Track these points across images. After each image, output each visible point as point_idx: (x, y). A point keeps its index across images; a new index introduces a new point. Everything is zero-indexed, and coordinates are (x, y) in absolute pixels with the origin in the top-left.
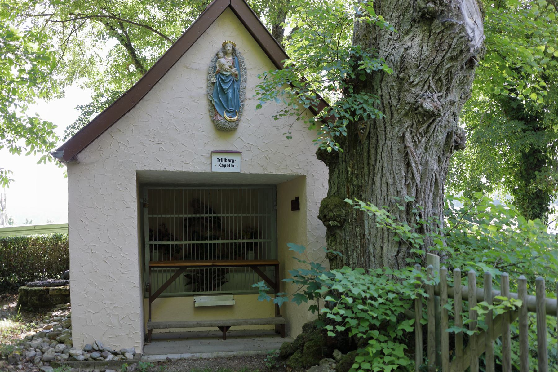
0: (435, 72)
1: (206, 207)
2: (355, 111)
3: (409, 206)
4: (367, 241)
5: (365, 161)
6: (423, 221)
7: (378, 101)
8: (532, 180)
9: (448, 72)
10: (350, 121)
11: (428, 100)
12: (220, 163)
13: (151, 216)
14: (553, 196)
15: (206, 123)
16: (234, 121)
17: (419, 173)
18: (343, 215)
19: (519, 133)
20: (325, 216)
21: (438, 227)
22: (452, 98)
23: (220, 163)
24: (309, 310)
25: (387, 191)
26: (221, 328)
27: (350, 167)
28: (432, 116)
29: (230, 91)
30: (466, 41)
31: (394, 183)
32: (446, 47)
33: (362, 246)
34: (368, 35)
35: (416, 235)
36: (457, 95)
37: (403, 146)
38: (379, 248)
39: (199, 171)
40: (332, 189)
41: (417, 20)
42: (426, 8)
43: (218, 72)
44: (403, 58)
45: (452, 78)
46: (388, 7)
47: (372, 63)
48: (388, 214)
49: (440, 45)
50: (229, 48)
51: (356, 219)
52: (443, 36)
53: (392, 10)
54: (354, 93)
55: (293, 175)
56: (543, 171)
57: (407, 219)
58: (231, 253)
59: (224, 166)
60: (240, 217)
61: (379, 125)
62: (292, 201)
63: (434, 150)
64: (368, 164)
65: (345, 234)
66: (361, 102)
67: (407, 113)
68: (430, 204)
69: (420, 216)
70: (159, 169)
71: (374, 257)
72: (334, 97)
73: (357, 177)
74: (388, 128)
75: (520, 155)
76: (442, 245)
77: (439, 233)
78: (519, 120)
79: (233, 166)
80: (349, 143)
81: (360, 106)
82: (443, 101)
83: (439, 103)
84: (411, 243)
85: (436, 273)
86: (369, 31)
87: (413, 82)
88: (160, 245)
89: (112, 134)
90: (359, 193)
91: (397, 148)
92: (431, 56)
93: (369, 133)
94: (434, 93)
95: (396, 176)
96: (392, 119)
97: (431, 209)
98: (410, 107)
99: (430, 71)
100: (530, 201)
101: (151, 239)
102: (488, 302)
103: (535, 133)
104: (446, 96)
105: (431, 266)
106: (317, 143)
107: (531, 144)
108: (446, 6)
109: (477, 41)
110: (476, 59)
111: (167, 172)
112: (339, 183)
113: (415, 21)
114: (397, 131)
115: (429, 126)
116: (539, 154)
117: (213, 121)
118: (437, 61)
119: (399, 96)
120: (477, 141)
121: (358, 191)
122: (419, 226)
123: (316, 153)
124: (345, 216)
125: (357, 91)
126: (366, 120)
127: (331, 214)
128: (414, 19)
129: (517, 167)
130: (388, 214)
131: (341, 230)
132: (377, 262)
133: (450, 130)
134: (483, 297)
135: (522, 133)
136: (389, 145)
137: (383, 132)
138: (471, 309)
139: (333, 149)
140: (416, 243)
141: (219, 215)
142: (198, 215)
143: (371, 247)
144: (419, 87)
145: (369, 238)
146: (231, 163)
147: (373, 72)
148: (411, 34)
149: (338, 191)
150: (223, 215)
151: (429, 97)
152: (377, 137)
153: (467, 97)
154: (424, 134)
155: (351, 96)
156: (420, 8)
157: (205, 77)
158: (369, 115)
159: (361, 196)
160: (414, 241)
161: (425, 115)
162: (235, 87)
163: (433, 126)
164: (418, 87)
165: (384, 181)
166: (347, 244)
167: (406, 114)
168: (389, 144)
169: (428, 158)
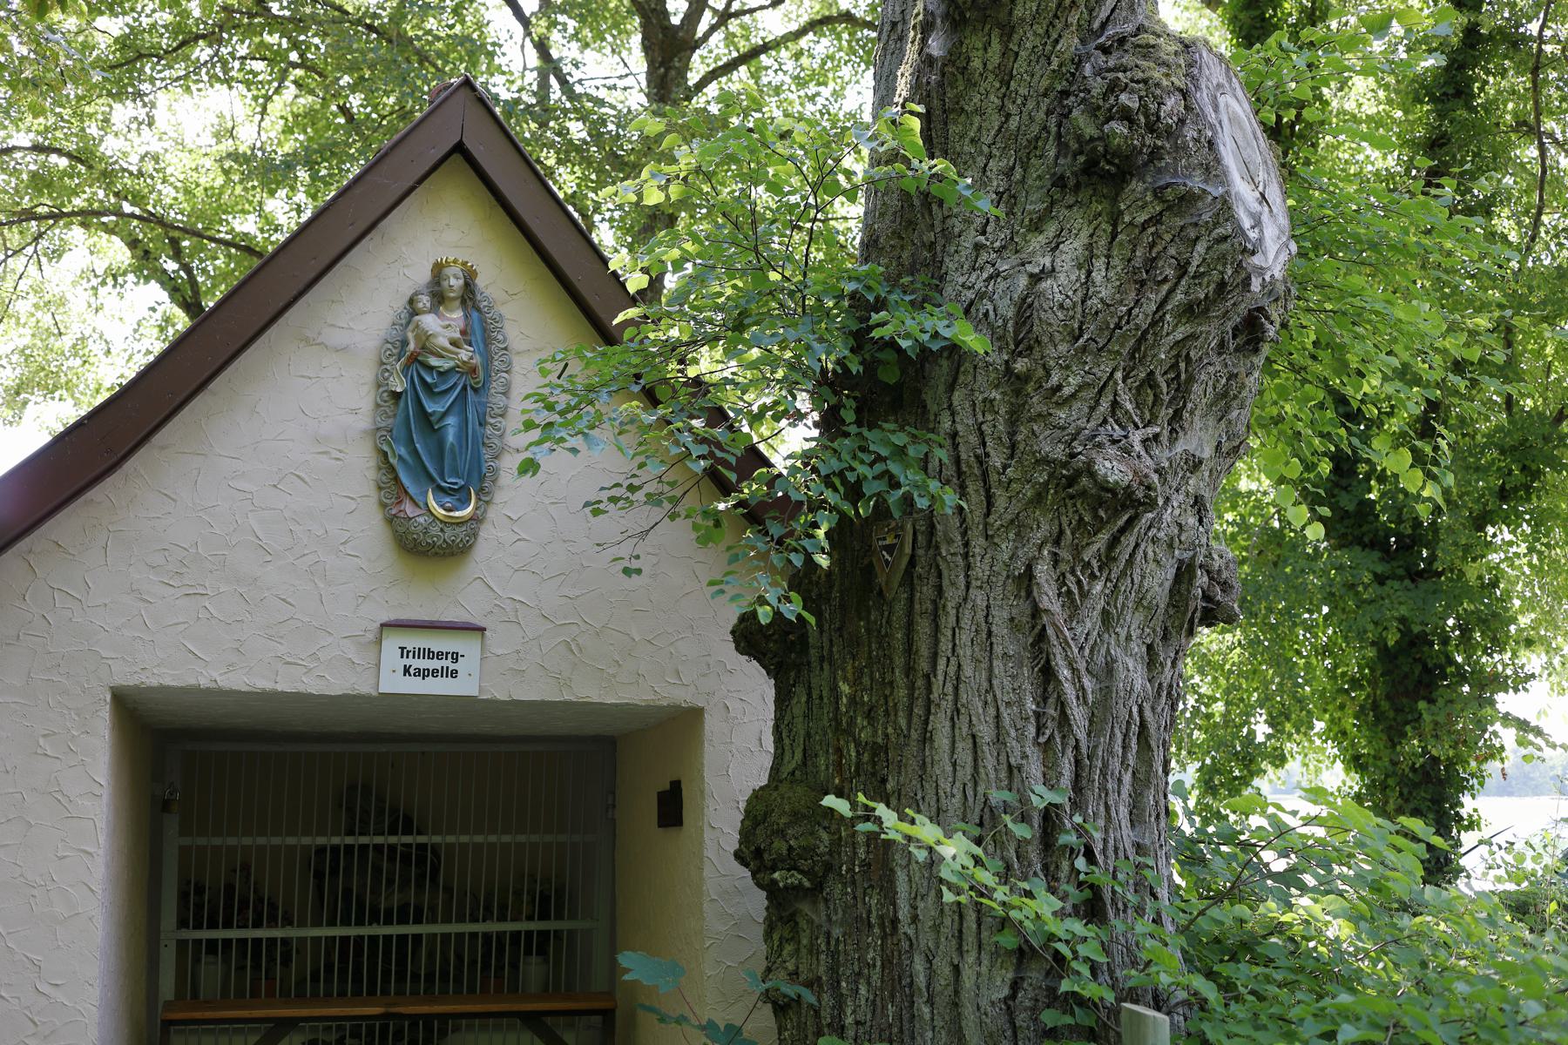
0: (1132, 357)
1: (394, 811)
2: (859, 482)
3: (1050, 818)
4: (905, 945)
5: (899, 661)
6: (1100, 876)
7: (942, 454)
8: (1408, 728)
9: (1178, 356)
11: (1112, 451)
12: (408, 662)
13: (186, 841)
14: (1473, 775)
16: (461, 523)
17: (1085, 702)
19: (1366, 587)
20: (758, 853)
21: (1154, 896)
22: (1191, 448)
23: (408, 662)
27: (845, 679)
28: (1124, 507)
29: (451, 421)
30: (1236, 249)
31: (999, 739)
32: (1170, 272)
33: (887, 963)
34: (910, 228)
35: (1077, 927)
36: (1206, 437)
37: (1026, 607)
38: (947, 971)
40: (787, 757)
41: (1072, 182)
42: (1099, 139)
43: (414, 359)
44: (1025, 309)
45: (1191, 379)
48: (979, 851)
49: (1151, 263)
50: (453, 281)
51: (866, 865)
52: (1156, 235)
53: (986, 149)
55: (661, 708)
56: (1441, 702)
57: (1045, 868)
59: (423, 674)
60: (492, 846)
61: (945, 534)
63: (1133, 621)
64: (909, 670)
65: (830, 920)
66: (884, 452)
68: (1124, 811)
70: (192, 681)
71: (930, 1001)
72: (789, 443)
73: (870, 715)
74: (978, 544)
75: (1371, 653)
76: (1169, 971)
77: (1157, 921)
78: (1364, 547)
79: (454, 674)
81: (879, 468)
82: (1163, 454)
83: (1149, 462)
84: (1058, 957)
86: (910, 222)
87: (1059, 387)
88: (227, 943)
89: (31, 558)
90: (876, 776)
91: (1006, 615)
92: (1121, 302)
93: (912, 562)
94: (1131, 428)
95: (1005, 713)
96: (988, 514)
98: (1051, 475)
100: (1405, 791)
101: (183, 923)
103: (1411, 586)
106: (722, 591)
107: (1403, 620)
108: (1169, 133)
109: (1271, 256)
110: (1267, 318)
111: (221, 692)
112: (808, 735)
114: (1006, 557)
115: (1114, 541)
116: (1426, 649)
117: (390, 520)
118: (1142, 318)
119: (1012, 434)
121: (874, 764)
122: (1088, 893)
123: (733, 632)
124: (830, 853)
125: (868, 415)
126: (896, 514)
127: (780, 846)
128: (1062, 177)
129: (1362, 687)
130: (979, 851)
131: (815, 903)
132: (939, 1023)
133: (1187, 555)
135: (1375, 585)
136: (977, 607)
139: (777, 614)
141: (437, 839)
142: (364, 840)
143: (919, 966)
145: (911, 932)
147: (924, 351)
148: (1051, 229)
149: (804, 764)
150: (451, 839)
151: (1114, 442)
152: (940, 576)
153: (1236, 449)
154: (1100, 569)
155: (846, 435)
156: (1079, 138)
157: (368, 374)
158: (908, 500)
159: (884, 781)
160: (1075, 952)
162: (470, 409)
163: (1129, 540)
164: (1076, 405)
165: (965, 730)
166: (834, 955)
167: (1039, 499)
168: (981, 602)
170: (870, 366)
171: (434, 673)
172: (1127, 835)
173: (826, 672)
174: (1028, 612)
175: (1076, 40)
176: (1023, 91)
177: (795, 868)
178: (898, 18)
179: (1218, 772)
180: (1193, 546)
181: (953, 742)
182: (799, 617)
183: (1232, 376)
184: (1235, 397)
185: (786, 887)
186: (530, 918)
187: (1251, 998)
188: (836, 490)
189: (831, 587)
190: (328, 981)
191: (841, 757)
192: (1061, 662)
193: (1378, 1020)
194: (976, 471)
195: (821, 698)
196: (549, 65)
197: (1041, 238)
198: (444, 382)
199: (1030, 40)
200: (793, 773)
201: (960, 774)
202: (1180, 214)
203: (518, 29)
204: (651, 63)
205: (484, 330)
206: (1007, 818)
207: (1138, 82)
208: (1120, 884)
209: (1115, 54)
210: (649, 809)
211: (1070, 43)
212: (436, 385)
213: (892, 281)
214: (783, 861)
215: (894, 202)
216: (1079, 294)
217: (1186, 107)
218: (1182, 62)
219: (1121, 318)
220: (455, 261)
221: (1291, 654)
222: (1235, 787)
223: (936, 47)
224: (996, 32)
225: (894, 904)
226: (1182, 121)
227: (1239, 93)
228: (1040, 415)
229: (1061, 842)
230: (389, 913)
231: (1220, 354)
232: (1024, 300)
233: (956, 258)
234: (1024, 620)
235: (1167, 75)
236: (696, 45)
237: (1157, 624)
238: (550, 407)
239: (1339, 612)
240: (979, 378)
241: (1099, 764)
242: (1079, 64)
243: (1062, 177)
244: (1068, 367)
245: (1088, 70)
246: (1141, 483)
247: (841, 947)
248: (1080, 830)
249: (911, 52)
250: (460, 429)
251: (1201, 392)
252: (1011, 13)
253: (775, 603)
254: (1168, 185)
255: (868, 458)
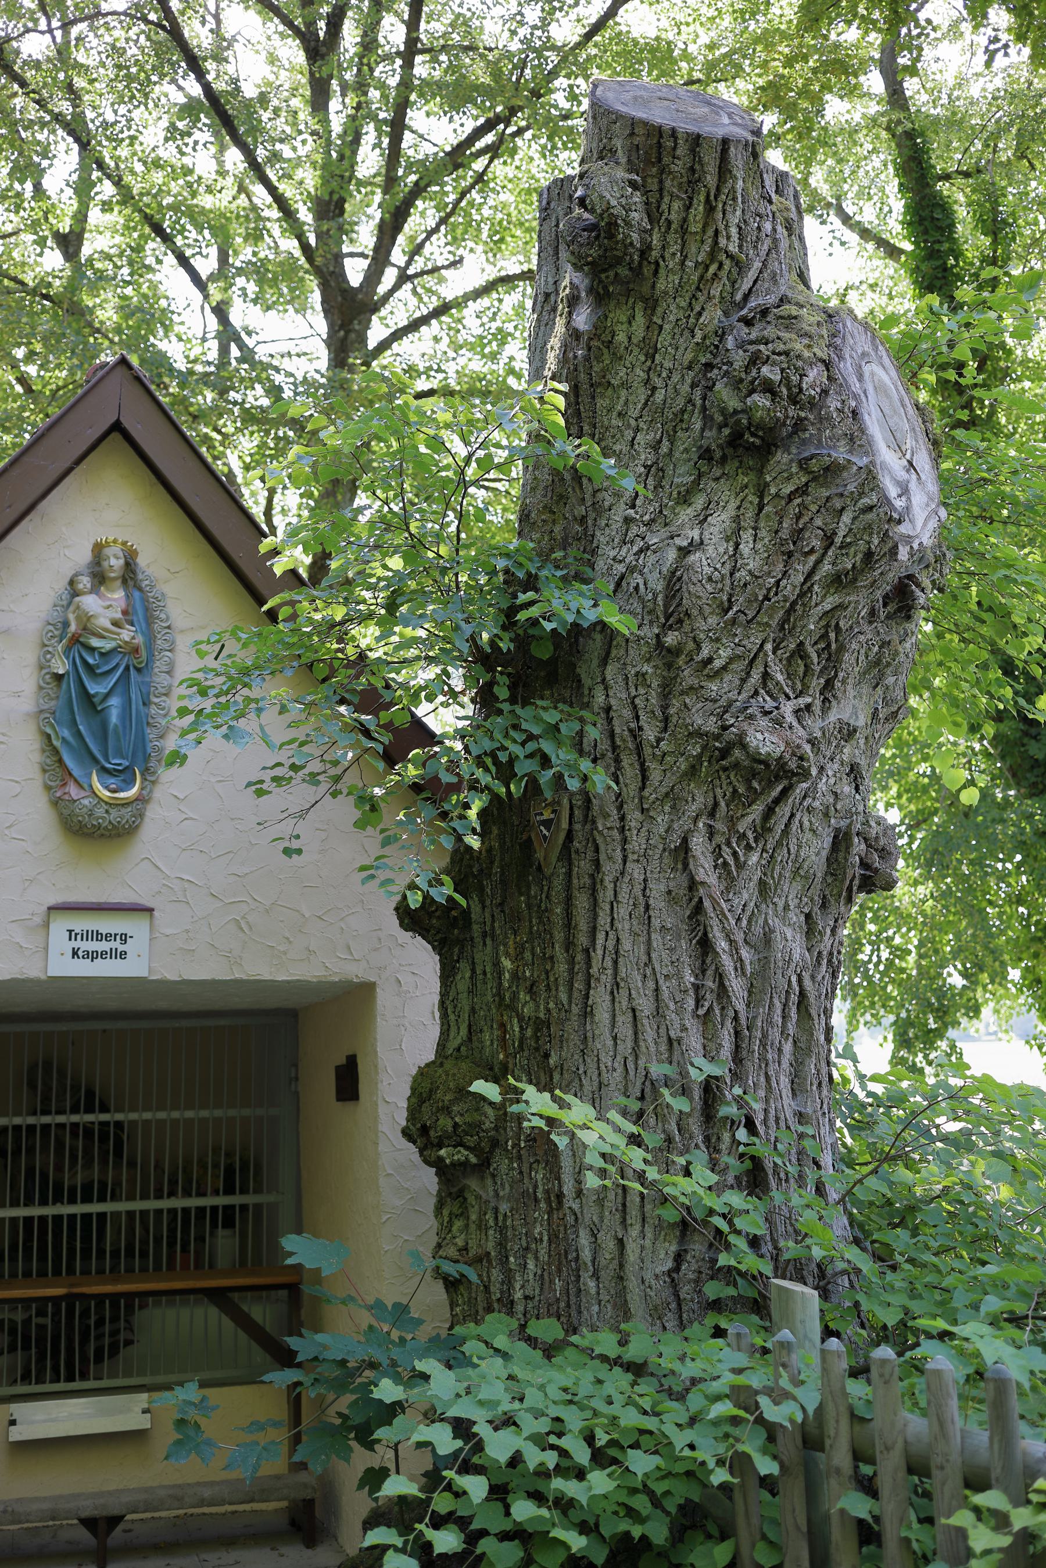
0: (782, 628)
1: (76, 1088)
3: (710, 1090)
4: (570, 1219)
5: (559, 936)
6: (761, 1149)
9: (827, 626)
10: (495, 797)
11: (763, 722)
12: (76, 944)
15: (32, 811)
16: (126, 804)
17: (744, 974)
18: (487, 1125)
22: (845, 717)
23: (76, 944)
24: (360, 1487)
25: (636, 1040)
26: (89, 1523)
27: (507, 955)
28: (778, 778)
29: (114, 701)
31: (658, 1012)
32: (816, 543)
33: (553, 1238)
34: (561, 507)
35: (736, 1199)
37: (683, 880)
39: (172, 976)
41: (718, 455)
42: (743, 411)
44: (674, 582)
45: (842, 648)
46: (620, 414)
47: (567, 598)
49: (797, 534)
50: (113, 562)
52: (803, 506)
53: (633, 423)
54: (512, 700)
57: (707, 1139)
58: (158, 1240)
59: (92, 956)
61: (601, 808)
62: (337, 1068)
63: (790, 891)
64: (569, 945)
65: (497, 1195)
66: (536, 731)
67: (693, 767)
68: (785, 1081)
69: (750, 1126)
71: (596, 1276)
73: (531, 990)
74: (634, 818)
79: (123, 955)
80: (502, 874)
81: (531, 746)
82: (815, 725)
83: (801, 732)
85: (803, 1371)
86: (561, 497)
87: (710, 660)
91: (663, 888)
92: (769, 574)
93: (570, 836)
95: (664, 986)
96: (643, 788)
97: (787, 1100)
98: (704, 748)
99: (767, 624)
102: (1006, 1490)
104: (825, 709)
105: (785, 1334)
106: (373, 877)
108: (812, 404)
109: (919, 524)
110: (918, 585)
112: (473, 1011)
113: (711, 459)
117: (55, 803)
118: (790, 589)
119: (664, 708)
120: (935, 859)
121: (537, 1039)
124: (496, 1128)
125: (522, 692)
126: (548, 794)
127: (445, 1123)
128: (708, 450)
131: (482, 1178)
132: (604, 1297)
133: (843, 824)
134: (988, 1469)
136: (634, 884)
137: (615, 833)
138: (943, 1521)
140: (738, 1232)
141: (119, 1117)
142: (46, 1119)
143: (584, 1240)
144: (730, 679)
145: (575, 1206)
146: (116, 944)
148: (699, 502)
149: (470, 1039)
151: (766, 713)
152: (597, 850)
154: (756, 840)
155: (500, 712)
156: (723, 411)
157: (30, 656)
158: (559, 777)
159: (547, 1056)
161: (754, 775)
163: (783, 811)
164: (727, 677)
165: (625, 1003)
167: (693, 771)
169: (774, 922)
170: (523, 642)
171: (103, 955)
172: (788, 1104)
173: (489, 948)
174: (685, 884)
175: (719, 313)
176: (668, 364)
177: (461, 1144)
178: (551, 289)
179: (912, 1025)
180: (850, 814)
181: (614, 1016)
182: (450, 899)
183: (884, 644)
184: (888, 664)
185: (453, 1164)
186: (216, 1193)
187: (907, 1266)
188: (487, 770)
189: (492, 862)
190: (28, 1258)
191: (505, 1032)
192: (718, 934)
193: (1027, 1288)
194: (630, 745)
195: (485, 973)
196: (228, 334)
197: (689, 511)
198: (107, 663)
199: (673, 312)
200: (458, 1049)
201: (620, 1048)
202: (825, 485)
203: (197, 295)
204: (331, 326)
205: (146, 609)
206: (665, 1091)
207: (779, 354)
208: (780, 1155)
209: (758, 326)
210: (328, 1083)
211: (713, 316)
212: (98, 666)
213: (544, 556)
214: (449, 1138)
215: (545, 477)
216: (728, 566)
217: (829, 378)
218: (825, 333)
219: (769, 590)
220: (115, 541)
221: (984, 904)
222: (930, 1038)
223: (582, 320)
224: (639, 306)
225: (559, 1179)
226: (825, 392)
227: (886, 361)
228: (691, 688)
229: (721, 1114)
230: (72, 1190)
231: (870, 623)
232: (673, 573)
233: (607, 531)
234: (682, 892)
235: (809, 346)
236: (375, 308)
237: (815, 892)
238: (203, 693)
239: (1030, 860)
240: (631, 652)
241: (759, 1035)
242: (722, 337)
243: (708, 450)
244: (718, 640)
245: (730, 342)
246: (794, 754)
247: (509, 1222)
248: (739, 1101)
249: (560, 326)
250: (124, 709)
251: (853, 661)
252: (653, 287)
253: (424, 886)
254: (812, 457)
255: (520, 737)
